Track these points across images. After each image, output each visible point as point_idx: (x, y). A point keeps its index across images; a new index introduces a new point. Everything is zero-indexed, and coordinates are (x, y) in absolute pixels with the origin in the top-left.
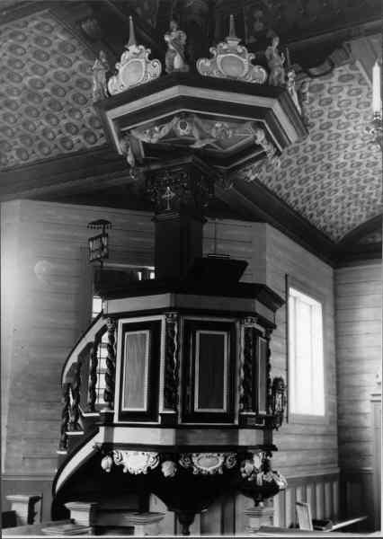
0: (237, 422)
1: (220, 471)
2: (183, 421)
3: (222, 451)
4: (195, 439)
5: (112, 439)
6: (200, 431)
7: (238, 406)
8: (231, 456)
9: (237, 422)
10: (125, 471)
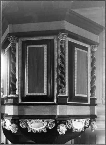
0: (55, 101)
1: (45, 131)
2: (22, 101)
3: (45, 119)
4: (29, 111)
5: (13, 108)
6: (32, 107)
7: (56, 92)
8: (51, 121)
9: (55, 101)
10: (29, 131)
